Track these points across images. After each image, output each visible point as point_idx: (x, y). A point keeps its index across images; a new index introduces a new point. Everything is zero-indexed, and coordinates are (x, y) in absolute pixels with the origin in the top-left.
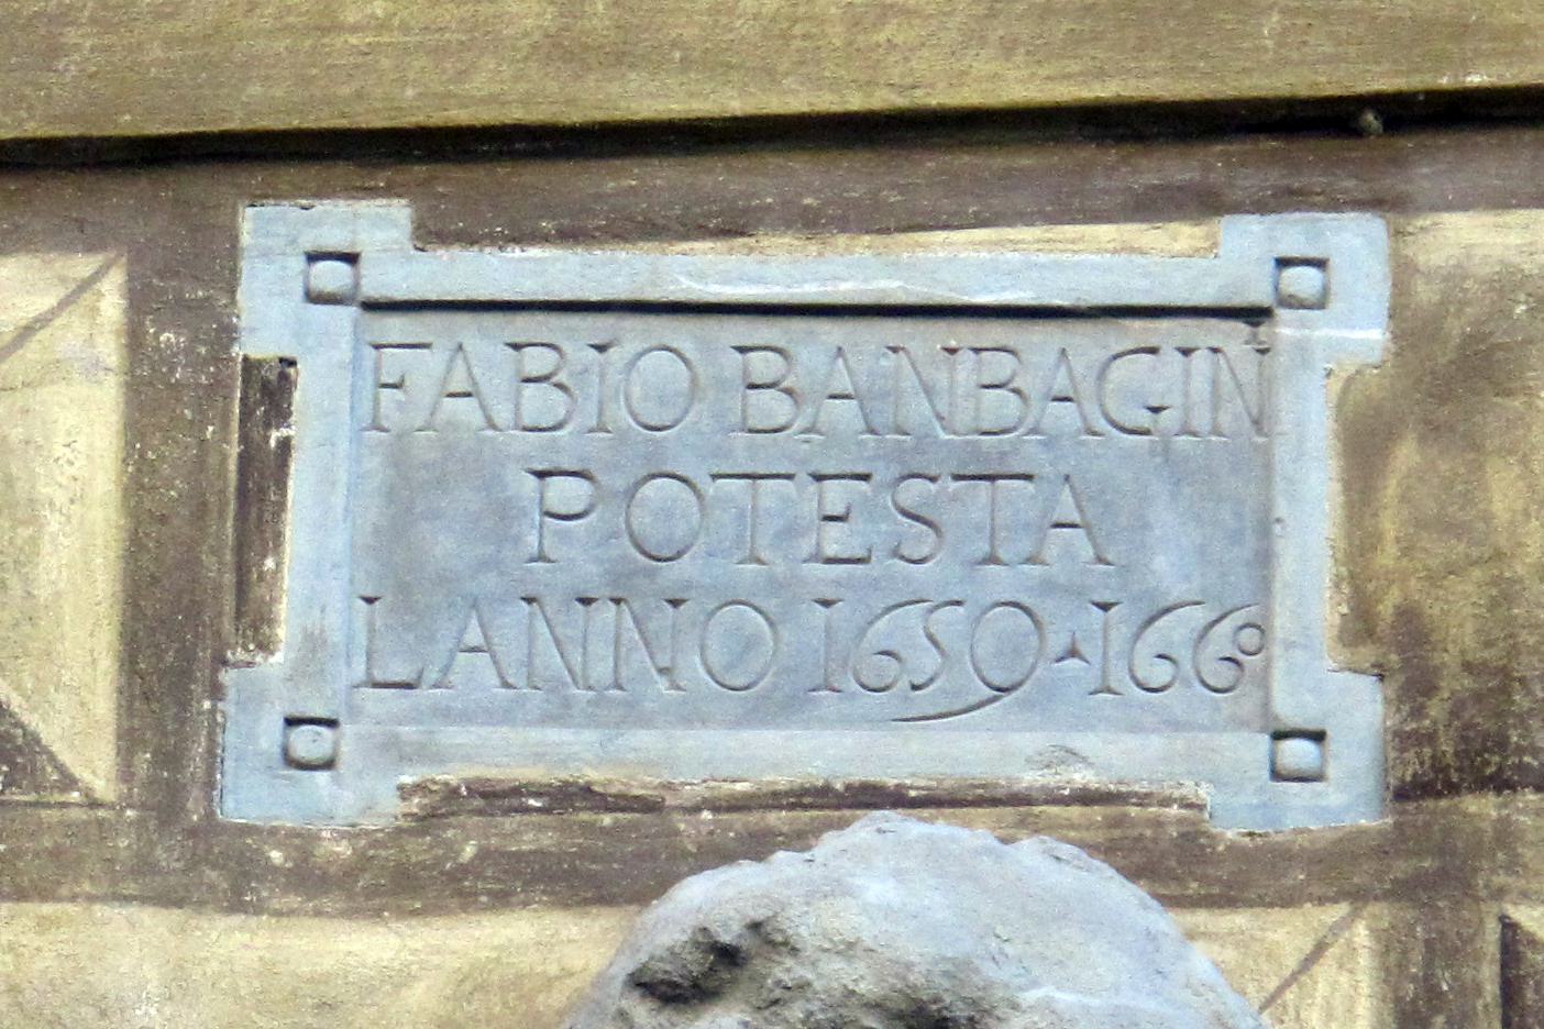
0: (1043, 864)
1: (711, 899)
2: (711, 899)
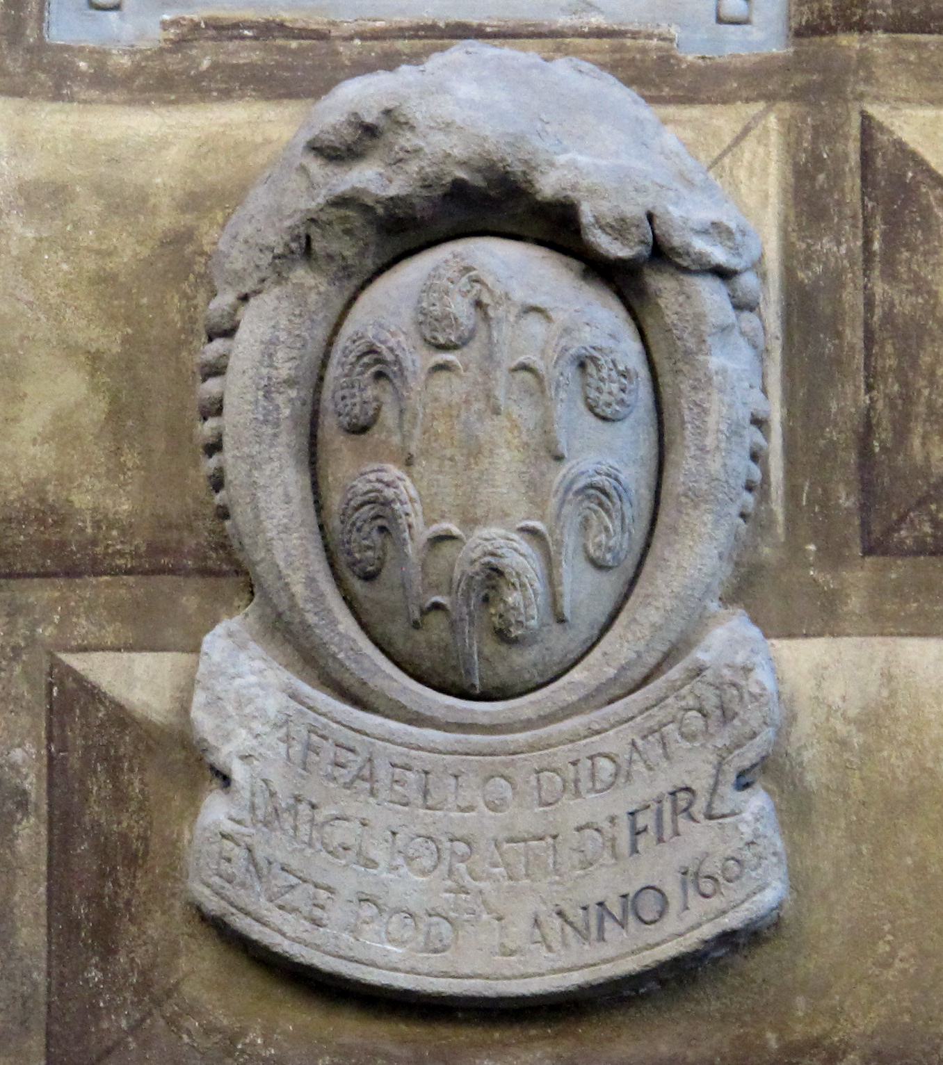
0: (574, 76)
1: (360, 95)
2: (360, 95)
